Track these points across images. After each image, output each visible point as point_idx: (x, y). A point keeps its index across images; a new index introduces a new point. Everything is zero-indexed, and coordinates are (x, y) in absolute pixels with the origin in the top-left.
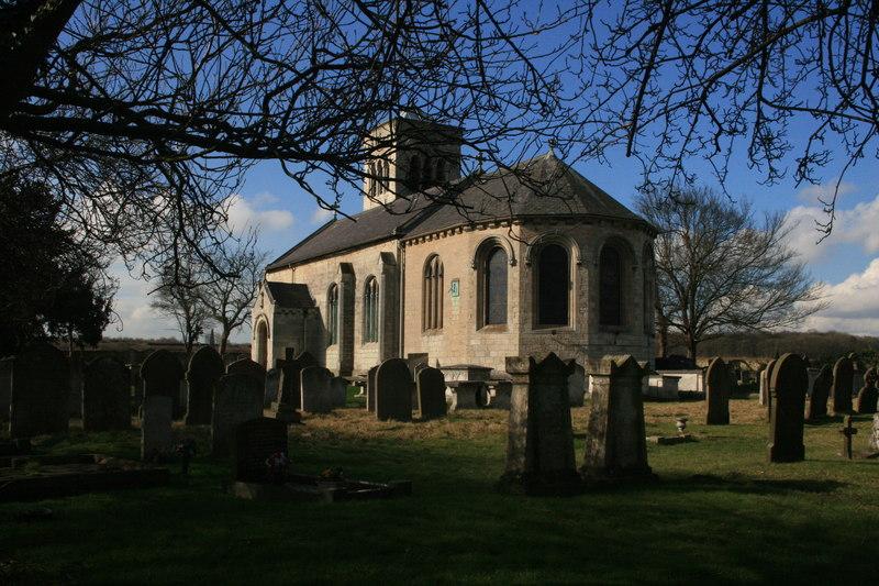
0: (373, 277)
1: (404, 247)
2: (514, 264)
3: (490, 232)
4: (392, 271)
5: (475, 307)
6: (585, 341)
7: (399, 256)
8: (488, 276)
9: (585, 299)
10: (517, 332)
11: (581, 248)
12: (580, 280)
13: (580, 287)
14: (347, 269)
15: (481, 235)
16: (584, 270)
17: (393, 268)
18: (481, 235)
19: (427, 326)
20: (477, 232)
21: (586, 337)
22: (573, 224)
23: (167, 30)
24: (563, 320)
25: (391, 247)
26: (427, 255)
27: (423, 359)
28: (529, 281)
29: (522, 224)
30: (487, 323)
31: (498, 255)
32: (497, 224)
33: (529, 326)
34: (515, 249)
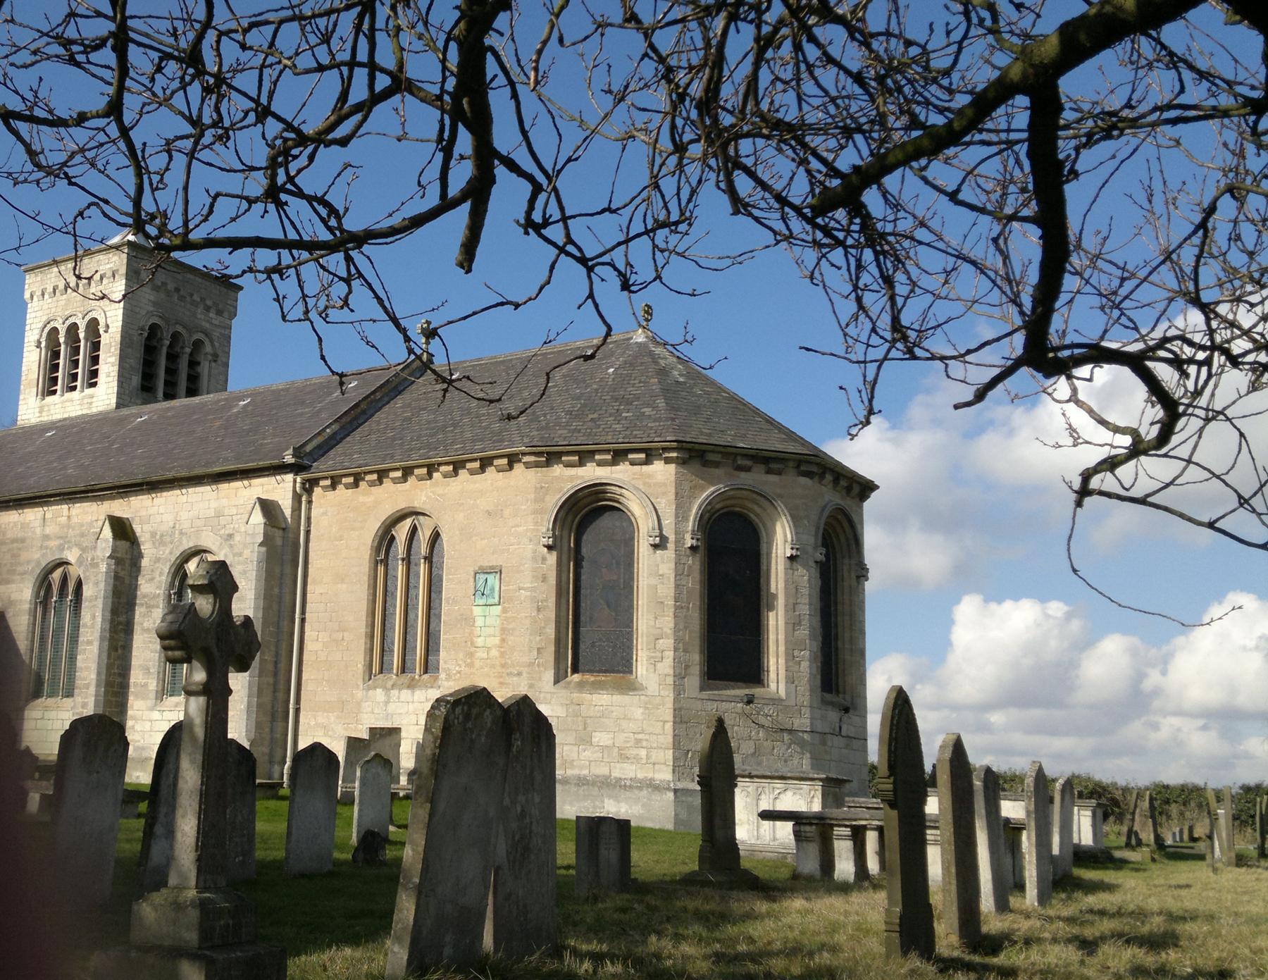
0: (63, 563)
1: (309, 492)
2: (660, 545)
3: (592, 473)
4: (279, 542)
5: (551, 631)
6: (803, 722)
7: (296, 509)
8: (578, 567)
9: (803, 632)
10: (669, 696)
11: (796, 521)
12: (793, 589)
13: (792, 607)
14: (121, 529)
15: (571, 478)
16: (801, 570)
17: (284, 545)
18: (571, 478)
19: (376, 667)
20: (558, 470)
21: (806, 713)
22: (779, 473)
23: (883, 236)
24: (752, 673)
25: (281, 489)
26: (387, 510)
27: (388, 741)
28: (694, 583)
29: (681, 462)
30: (575, 670)
31: (605, 521)
32: (619, 456)
33: (694, 681)
34: (665, 523)
